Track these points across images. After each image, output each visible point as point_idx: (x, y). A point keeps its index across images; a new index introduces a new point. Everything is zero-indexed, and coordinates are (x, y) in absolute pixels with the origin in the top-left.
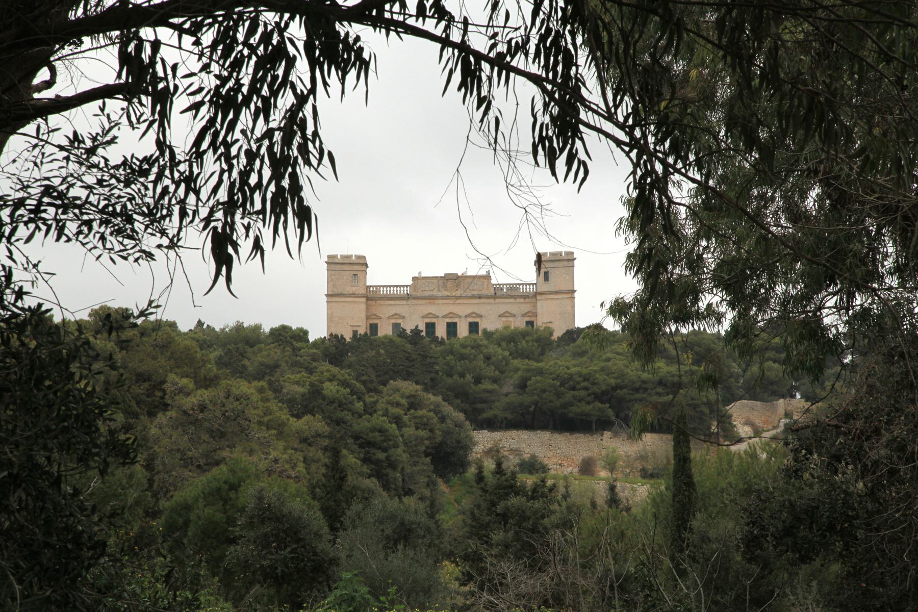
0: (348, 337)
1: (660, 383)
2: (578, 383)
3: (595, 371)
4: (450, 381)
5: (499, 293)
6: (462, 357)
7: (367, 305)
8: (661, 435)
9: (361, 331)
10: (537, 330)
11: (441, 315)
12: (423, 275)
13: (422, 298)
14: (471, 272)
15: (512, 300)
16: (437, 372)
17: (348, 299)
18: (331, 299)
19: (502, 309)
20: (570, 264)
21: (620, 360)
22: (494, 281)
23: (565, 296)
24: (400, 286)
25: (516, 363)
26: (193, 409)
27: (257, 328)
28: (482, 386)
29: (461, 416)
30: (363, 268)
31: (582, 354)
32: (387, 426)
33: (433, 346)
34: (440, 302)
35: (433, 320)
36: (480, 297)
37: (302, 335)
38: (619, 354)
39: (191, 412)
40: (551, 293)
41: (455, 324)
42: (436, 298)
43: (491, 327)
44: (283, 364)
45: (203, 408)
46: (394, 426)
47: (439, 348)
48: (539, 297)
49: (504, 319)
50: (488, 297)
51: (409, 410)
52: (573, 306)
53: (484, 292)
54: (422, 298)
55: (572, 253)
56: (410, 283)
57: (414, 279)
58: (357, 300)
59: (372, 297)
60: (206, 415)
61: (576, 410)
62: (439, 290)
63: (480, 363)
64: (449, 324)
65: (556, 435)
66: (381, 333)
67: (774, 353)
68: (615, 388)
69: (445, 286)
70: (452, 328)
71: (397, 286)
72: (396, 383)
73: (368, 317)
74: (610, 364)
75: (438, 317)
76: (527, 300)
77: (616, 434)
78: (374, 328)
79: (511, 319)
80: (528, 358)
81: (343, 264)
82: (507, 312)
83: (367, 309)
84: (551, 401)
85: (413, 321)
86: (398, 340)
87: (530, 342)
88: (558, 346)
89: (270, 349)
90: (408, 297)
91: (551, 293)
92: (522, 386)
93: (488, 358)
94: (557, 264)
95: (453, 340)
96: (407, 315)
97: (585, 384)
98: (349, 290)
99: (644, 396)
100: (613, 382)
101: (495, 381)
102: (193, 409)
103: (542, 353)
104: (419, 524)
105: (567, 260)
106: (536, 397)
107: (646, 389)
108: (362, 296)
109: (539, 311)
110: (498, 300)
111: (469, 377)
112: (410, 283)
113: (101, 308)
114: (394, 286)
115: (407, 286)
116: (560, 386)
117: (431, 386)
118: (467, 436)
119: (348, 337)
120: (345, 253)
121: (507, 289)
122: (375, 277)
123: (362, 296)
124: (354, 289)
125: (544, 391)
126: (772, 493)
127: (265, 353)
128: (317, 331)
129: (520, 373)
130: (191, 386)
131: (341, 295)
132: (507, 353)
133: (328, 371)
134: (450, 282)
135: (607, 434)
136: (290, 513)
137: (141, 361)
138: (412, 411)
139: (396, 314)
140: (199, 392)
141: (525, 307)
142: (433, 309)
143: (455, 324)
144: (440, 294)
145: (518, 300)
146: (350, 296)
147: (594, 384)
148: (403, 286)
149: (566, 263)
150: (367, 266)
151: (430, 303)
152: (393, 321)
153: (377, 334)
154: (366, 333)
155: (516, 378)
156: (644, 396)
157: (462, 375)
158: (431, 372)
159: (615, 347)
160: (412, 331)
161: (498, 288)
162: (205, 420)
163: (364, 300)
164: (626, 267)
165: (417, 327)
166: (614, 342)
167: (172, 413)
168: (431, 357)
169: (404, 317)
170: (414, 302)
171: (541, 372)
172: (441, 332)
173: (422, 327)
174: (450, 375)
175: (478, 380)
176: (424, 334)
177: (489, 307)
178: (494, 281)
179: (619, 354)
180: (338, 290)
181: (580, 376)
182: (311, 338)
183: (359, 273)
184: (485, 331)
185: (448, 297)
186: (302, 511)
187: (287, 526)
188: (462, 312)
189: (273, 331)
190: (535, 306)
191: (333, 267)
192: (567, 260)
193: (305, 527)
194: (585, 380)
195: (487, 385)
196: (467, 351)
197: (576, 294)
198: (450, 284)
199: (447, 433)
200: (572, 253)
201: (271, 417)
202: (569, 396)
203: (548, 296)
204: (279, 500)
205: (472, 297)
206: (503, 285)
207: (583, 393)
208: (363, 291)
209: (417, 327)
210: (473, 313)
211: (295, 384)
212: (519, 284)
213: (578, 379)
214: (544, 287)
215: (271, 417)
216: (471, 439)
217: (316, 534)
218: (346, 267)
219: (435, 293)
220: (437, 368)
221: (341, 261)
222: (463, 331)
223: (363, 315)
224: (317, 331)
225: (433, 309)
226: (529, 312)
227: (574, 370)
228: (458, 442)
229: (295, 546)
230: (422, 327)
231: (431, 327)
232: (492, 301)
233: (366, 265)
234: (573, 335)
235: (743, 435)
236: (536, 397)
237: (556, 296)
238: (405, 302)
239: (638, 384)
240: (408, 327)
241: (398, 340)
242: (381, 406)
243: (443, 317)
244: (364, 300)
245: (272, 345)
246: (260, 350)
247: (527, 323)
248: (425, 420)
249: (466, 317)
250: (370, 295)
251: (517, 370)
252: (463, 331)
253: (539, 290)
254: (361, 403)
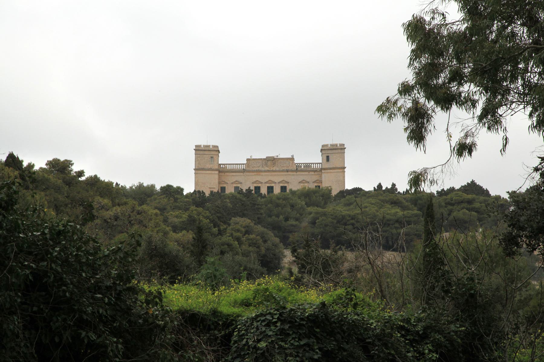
0: (207, 194)
1: (397, 221)
3: (358, 214)
4: (270, 220)
5: (299, 169)
6: (278, 205)
7: (219, 176)
9: (216, 190)
10: (322, 189)
12: (253, 158)
13: (253, 171)
14: (281, 156)
15: (307, 173)
16: (261, 214)
17: (208, 172)
18: (197, 172)
19: (301, 178)
20: (342, 151)
21: (373, 207)
22: (295, 162)
23: (339, 171)
24: (239, 164)
25: (309, 209)
26: (110, 219)
27: (153, 186)
29: (277, 240)
30: (217, 153)
31: (349, 204)
32: (232, 242)
33: (259, 199)
34: (263, 174)
35: (259, 185)
36: (287, 171)
37: (180, 190)
38: (372, 204)
39: (109, 221)
40: (330, 169)
41: (272, 187)
42: (261, 171)
43: (295, 189)
44: (168, 208)
45: (116, 218)
46: (236, 243)
47: (263, 200)
48: (323, 171)
49: (302, 184)
50: (292, 171)
51: (245, 235)
52: (344, 177)
53: (290, 168)
54: (253, 171)
55: (344, 145)
56: (245, 162)
57: (248, 160)
58: (213, 172)
59: (222, 171)
60: (119, 223)
62: (263, 167)
63: (289, 209)
64: (268, 187)
66: (228, 191)
67: (466, 204)
69: (266, 164)
70: (270, 189)
71: (237, 164)
72: (236, 219)
73: (219, 183)
74: (367, 209)
75: (262, 183)
76: (316, 173)
78: (223, 189)
79: (306, 184)
80: (317, 206)
81: (205, 150)
82: (304, 180)
83: (219, 178)
84: (330, 232)
85: (247, 184)
86: (238, 196)
87: (317, 197)
88: (335, 200)
89: (160, 199)
90: (244, 171)
91: (330, 169)
92: (313, 223)
93: (292, 206)
95: (271, 195)
98: (208, 166)
99: (388, 229)
101: (297, 220)
102: (110, 219)
103: (326, 203)
104: (256, 270)
105: (340, 149)
106: (322, 229)
107: (389, 225)
108: (216, 170)
109: (323, 179)
110: (298, 173)
111: (281, 217)
112: (245, 162)
113: (54, 160)
114: (235, 164)
115: (243, 164)
116: (337, 223)
117: (259, 221)
118: (280, 252)
119: (207, 194)
120: (206, 144)
121: (304, 166)
122: (223, 159)
123: (216, 170)
124: (211, 166)
125: (326, 225)
126: (528, 203)
127: (157, 201)
128: (189, 188)
129: (312, 215)
130: (110, 204)
131: (203, 169)
132: (304, 203)
133: (196, 210)
134: (269, 162)
136: (170, 252)
137: (79, 193)
138: (247, 235)
139: (236, 181)
140: (115, 208)
141: (315, 178)
142: (259, 178)
143: (272, 187)
144: (263, 169)
145: (311, 173)
146: (209, 170)
148: (241, 164)
149: (340, 151)
150: (219, 152)
151: (257, 175)
152: (235, 185)
153: (225, 192)
154: (218, 191)
155: (309, 218)
156: (388, 229)
157: (278, 216)
158: (257, 214)
159: (370, 199)
160: (246, 190)
161: (298, 166)
162: (118, 226)
163: (217, 172)
164: (411, 59)
165: (249, 188)
166: (369, 197)
167: (98, 221)
168: (258, 205)
169: (241, 183)
171: (325, 214)
172: (264, 191)
173: (252, 188)
174: (270, 216)
175: (287, 219)
176: (253, 192)
177: (293, 177)
178: (295, 162)
179: (372, 204)
180: (200, 167)
181: (350, 217)
182: (185, 193)
183: (214, 156)
184: (291, 190)
185: (268, 171)
186: (179, 251)
187: (167, 261)
189: (162, 188)
190: (321, 177)
191: (199, 152)
192: (340, 149)
193: (180, 262)
194: (352, 219)
195: (292, 222)
196: (280, 201)
197: (346, 170)
198: (269, 163)
199: (268, 249)
200: (344, 145)
201: (159, 228)
202: (341, 229)
203: (329, 171)
204: (162, 243)
205: (283, 171)
206: (302, 164)
208: (217, 167)
209: (249, 188)
210: (283, 181)
211: (176, 217)
212: (311, 164)
213: (348, 218)
214: (327, 165)
215: (159, 228)
216: (283, 253)
217: (188, 267)
218: (206, 153)
219: (260, 168)
220: (262, 211)
221: (203, 149)
222: (277, 190)
223: (217, 181)
224: (189, 188)
225: (259, 178)
226: (317, 180)
227: (344, 213)
228: (275, 255)
229: (173, 274)
230: (252, 188)
231: (258, 189)
232: (295, 173)
233: (219, 151)
234: (344, 193)
236: (322, 229)
237: (334, 171)
238: (242, 174)
240: (244, 188)
241: (238, 196)
242: (229, 231)
244: (217, 172)
245: (163, 196)
246: (155, 199)
247: (316, 186)
248: (255, 241)
249: (279, 183)
250: (221, 170)
251: (310, 213)
252: (277, 190)
254: (217, 229)
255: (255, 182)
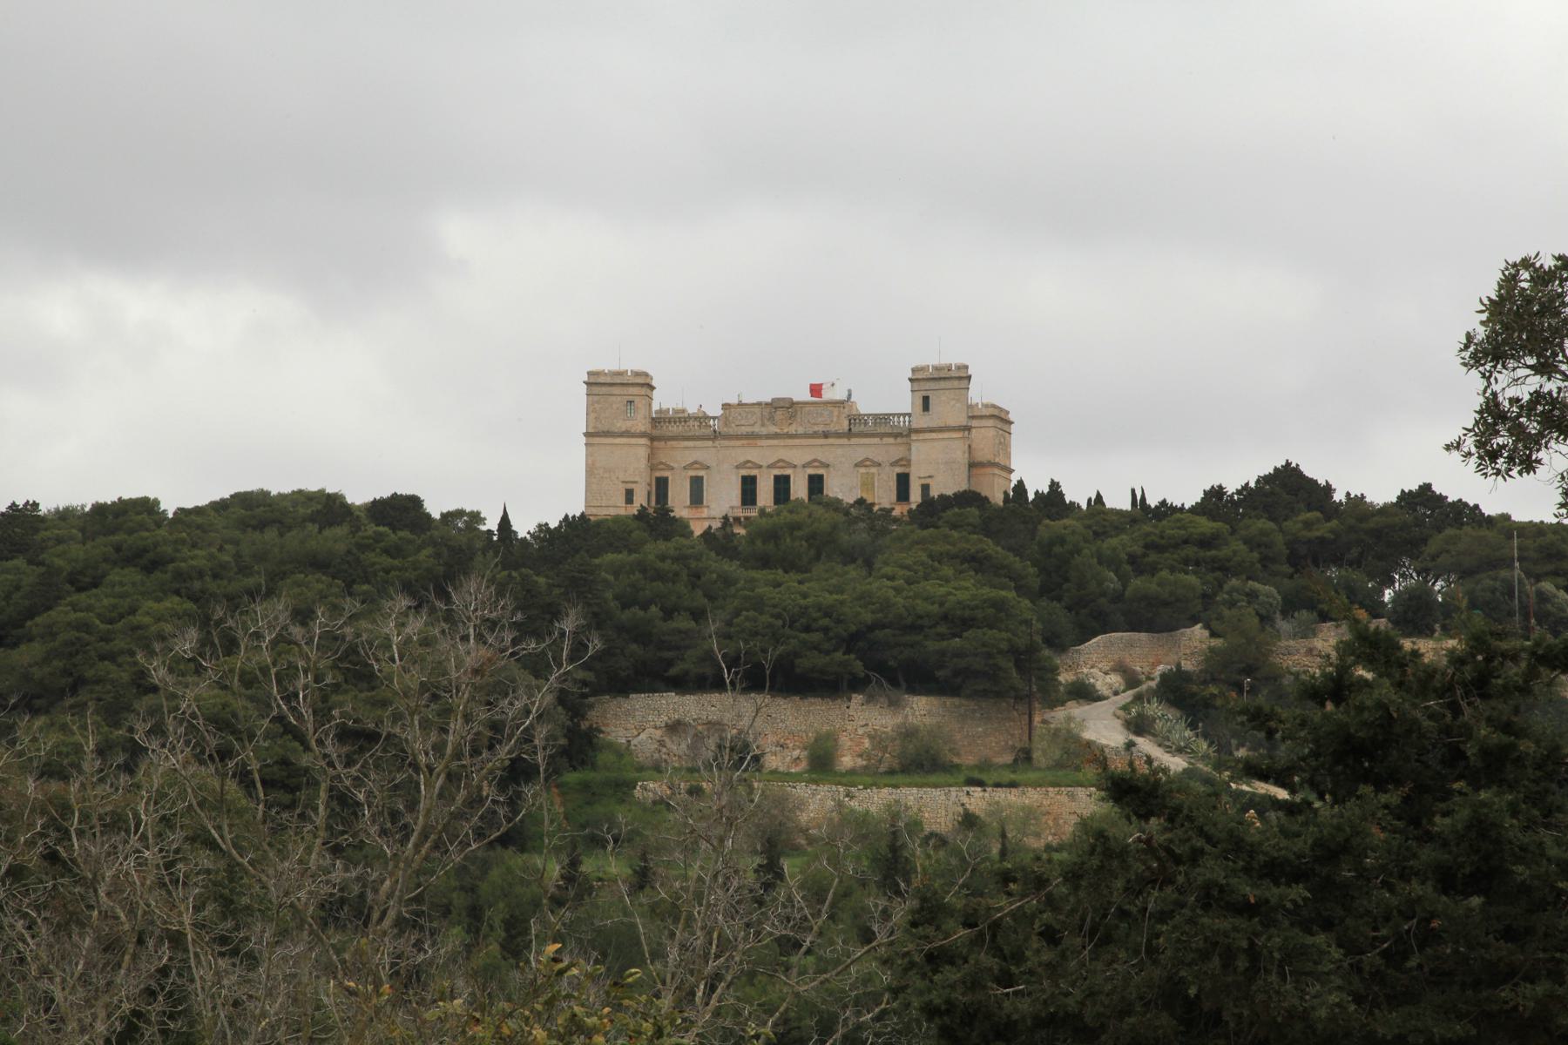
1: (945, 617)
2: (815, 620)
6: (660, 576)
8: (943, 699)
11: (764, 464)
15: (876, 440)
17: (618, 441)
20: (963, 384)
28: (673, 624)
30: (644, 391)
35: (753, 472)
36: (826, 435)
40: (932, 430)
41: (787, 478)
48: (914, 437)
49: (862, 470)
53: (833, 428)
55: (966, 367)
57: (726, 406)
58: (633, 441)
59: (665, 430)
61: (807, 662)
64: (777, 478)
65: (780, 701)
68: (872, 628)
69: (771, 419)
73: (652, 468)
76: (899, 440)
77: (870, 699)
79: (874, 470)
91: (932, 430)
94: (943, 384)
96: (713, 464)
97: (826, 622)
98: (621, 425)
100: (868, 617)
107: (922, 628)
108: (642, 435)
109: (913, 458)
110: (854, 441)
123: (642, 435)
131: (607, 434)
134: (779, 412)
135: (857, 698)
141: (897, 452)
142: (753, 455)
143: (787, 478)
144: (764, 431)
147: (839, 621)
149: (956, 383)
151: (749, 445)
170: (726, 443)
175: (668, 614)
177: (840, 451)
183: (637, 399)
185: (776, 436)
188: (798, 458)
191: (596, 390)
194: (827, 615)
195: (683, 623)
205: (815, 435)
207: (816, 637)
213: (815, 615)
214: (921, 421)
218: (616, 390)
219: (757, 429)
222: (799, 490)
225: (753, 455)
232: (844, 441)
235: (1105, 691)
237: (940, 436)
239: (909, 621)
243: (770, 467)
244: (643, 441)
252: (799, 490)
253: (914, 426)
255: (745, 464)
